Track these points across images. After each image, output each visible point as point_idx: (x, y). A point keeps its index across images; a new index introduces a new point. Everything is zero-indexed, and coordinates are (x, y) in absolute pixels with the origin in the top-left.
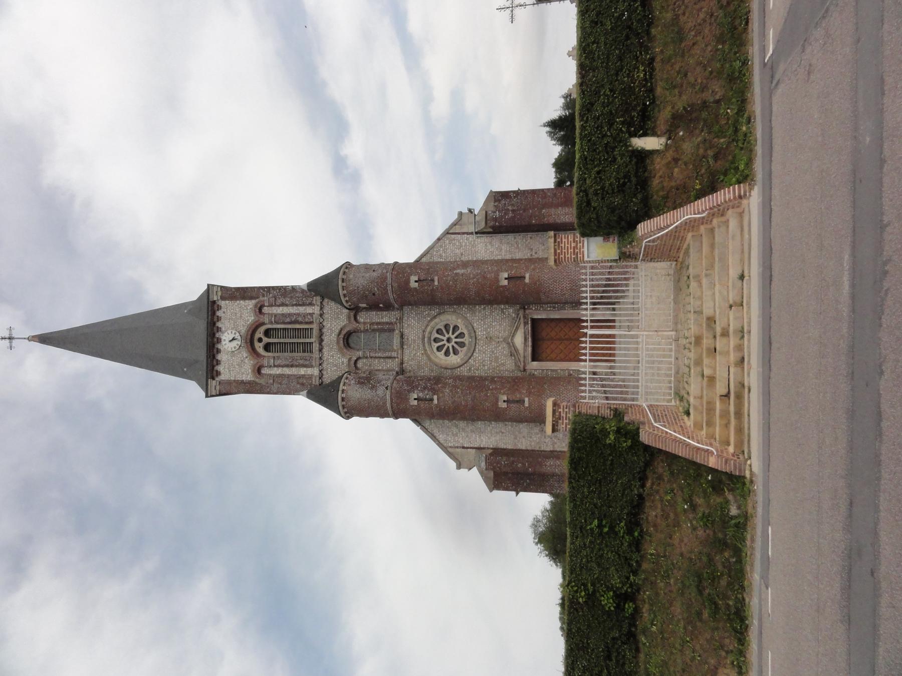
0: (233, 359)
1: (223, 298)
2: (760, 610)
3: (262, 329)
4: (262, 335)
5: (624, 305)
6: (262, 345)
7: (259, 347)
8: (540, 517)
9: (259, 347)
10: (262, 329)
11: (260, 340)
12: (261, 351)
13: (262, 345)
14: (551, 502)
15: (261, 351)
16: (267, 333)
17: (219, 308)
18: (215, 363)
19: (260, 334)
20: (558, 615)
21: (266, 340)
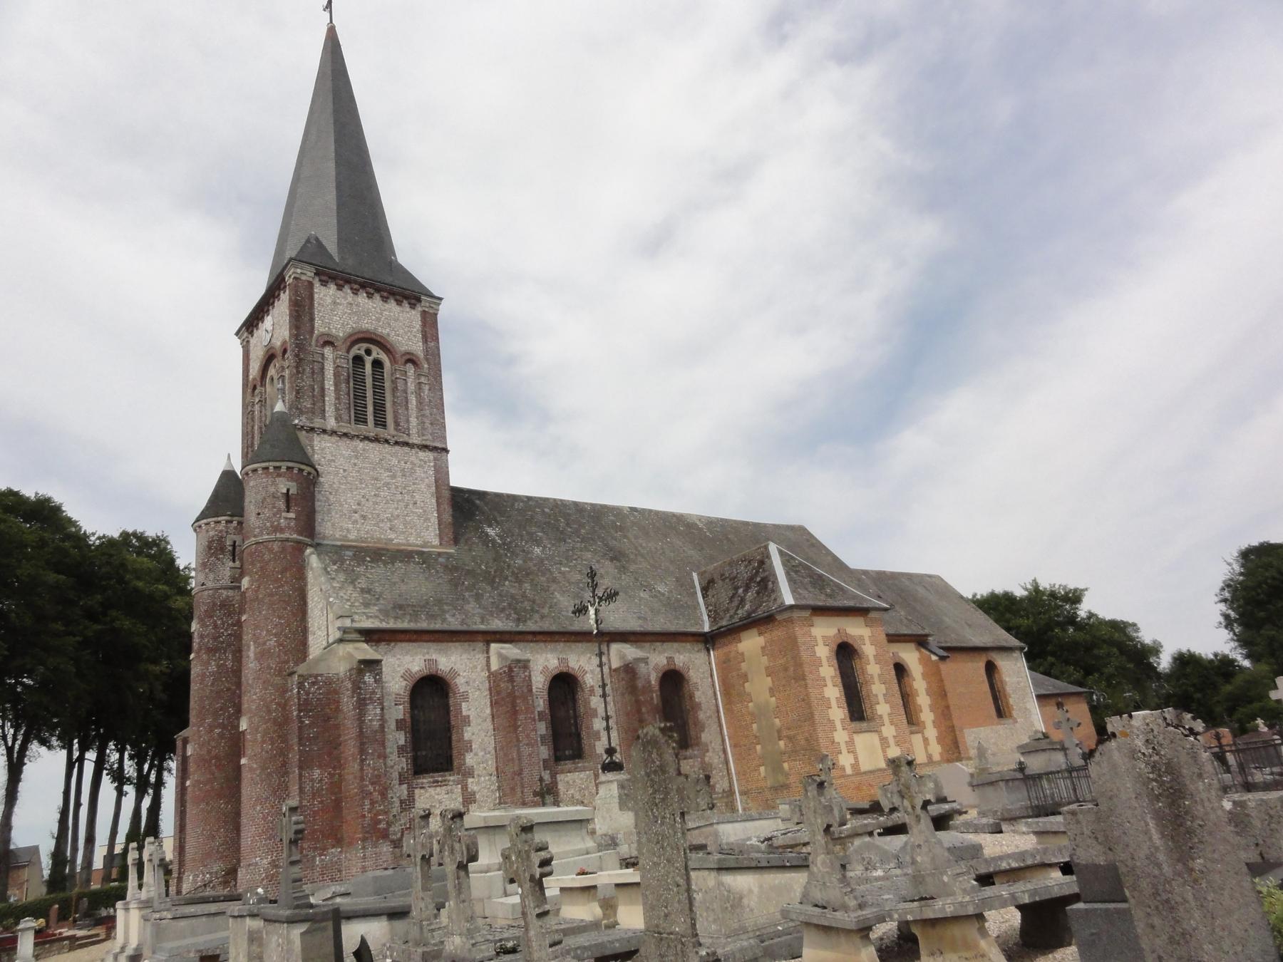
0: (339, 311)
1: (424, 313)
2: (234, 822)
3: (383, 357)
4: (374, 355)
5: (756, 534)
6: (362, 352)
7: (359, 350)
8: (1140, 635)
9: (359, 350)
10: (383, 357)
11: (368, 352)
12: (355, 351)
13: (362, 352)
14: (1155, 650)
15: (355, 351)
16: (377, 364)
17: (413, 306)
18: (324, 278)
19: (377, 353)
20: (81, 523)
21: (368, 361)
